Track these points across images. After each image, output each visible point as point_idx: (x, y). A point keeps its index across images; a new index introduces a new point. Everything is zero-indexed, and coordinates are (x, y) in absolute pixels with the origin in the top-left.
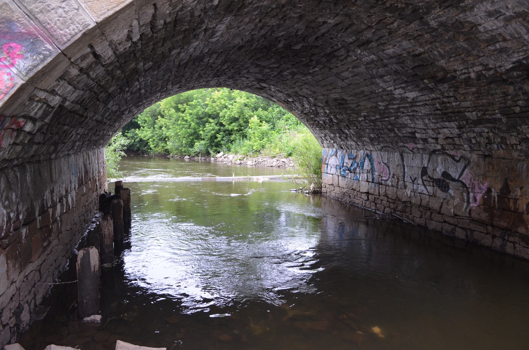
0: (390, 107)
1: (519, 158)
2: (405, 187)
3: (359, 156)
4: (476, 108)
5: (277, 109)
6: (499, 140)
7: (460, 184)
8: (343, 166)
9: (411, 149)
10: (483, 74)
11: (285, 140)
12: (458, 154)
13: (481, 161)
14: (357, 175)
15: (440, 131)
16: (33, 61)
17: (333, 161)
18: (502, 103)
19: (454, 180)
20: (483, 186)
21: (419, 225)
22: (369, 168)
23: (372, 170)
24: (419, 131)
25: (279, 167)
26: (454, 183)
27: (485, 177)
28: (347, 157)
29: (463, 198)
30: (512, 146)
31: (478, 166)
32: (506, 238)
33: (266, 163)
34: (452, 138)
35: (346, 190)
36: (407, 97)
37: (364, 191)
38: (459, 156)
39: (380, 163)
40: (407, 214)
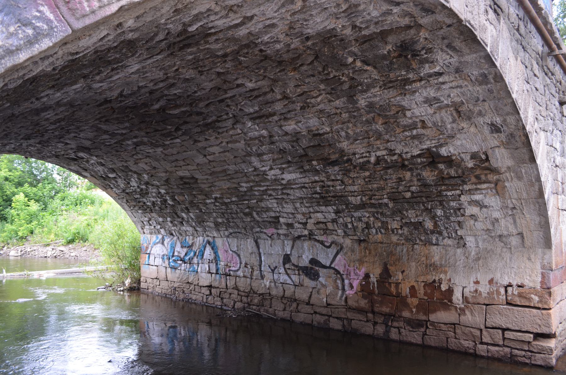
0: (256, 189)
1: (399, 242)
2: (262, 277)
3: (197, 244)
4: (363, 193)
5: (50, 185)
6: (380, 225)
7: (332, 271)
8: (173, 256)
9: (270, 235)
10: (384, 159)
11: (62, 222)
12: (330, 239)
13: (356, 247)
14: (195, 266)
15: (312, 215)
16: (8, 38)
17: (158, 250)
18: (393, 188)
19: (324, 267)
20: (360, 271)
21: (283, 320)
22: (212, 257)
23: (216, 260)
24: (285, 215)
25: (56, 257)
26: (325, 270)
27: (361, 262)
28: (179, 244)
29: (337, 286)
30: (393, 231)
31: (353, 251)
32: (390, 324)
33: (36, 253)
34: (325, 223)
35: (178, 284)
36: (283, 179)
37: (205, 284)
38: (330, 241)
39: (227, 251)
40: (266, 308)
